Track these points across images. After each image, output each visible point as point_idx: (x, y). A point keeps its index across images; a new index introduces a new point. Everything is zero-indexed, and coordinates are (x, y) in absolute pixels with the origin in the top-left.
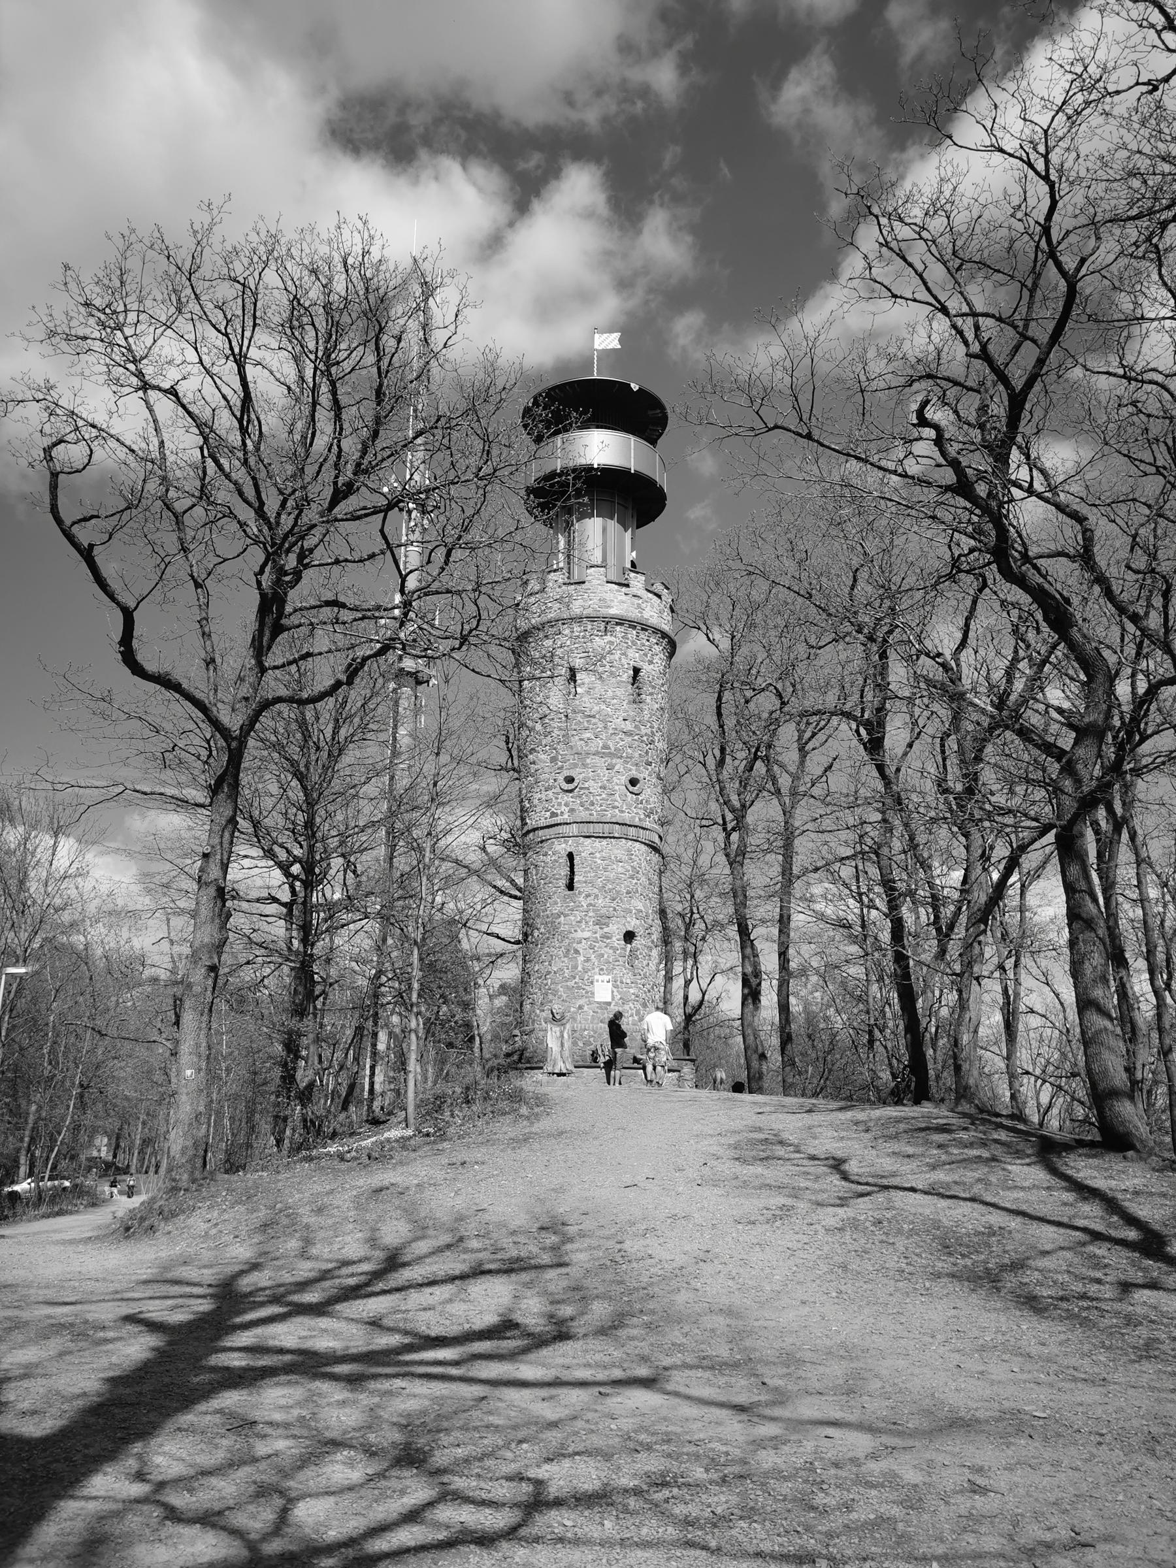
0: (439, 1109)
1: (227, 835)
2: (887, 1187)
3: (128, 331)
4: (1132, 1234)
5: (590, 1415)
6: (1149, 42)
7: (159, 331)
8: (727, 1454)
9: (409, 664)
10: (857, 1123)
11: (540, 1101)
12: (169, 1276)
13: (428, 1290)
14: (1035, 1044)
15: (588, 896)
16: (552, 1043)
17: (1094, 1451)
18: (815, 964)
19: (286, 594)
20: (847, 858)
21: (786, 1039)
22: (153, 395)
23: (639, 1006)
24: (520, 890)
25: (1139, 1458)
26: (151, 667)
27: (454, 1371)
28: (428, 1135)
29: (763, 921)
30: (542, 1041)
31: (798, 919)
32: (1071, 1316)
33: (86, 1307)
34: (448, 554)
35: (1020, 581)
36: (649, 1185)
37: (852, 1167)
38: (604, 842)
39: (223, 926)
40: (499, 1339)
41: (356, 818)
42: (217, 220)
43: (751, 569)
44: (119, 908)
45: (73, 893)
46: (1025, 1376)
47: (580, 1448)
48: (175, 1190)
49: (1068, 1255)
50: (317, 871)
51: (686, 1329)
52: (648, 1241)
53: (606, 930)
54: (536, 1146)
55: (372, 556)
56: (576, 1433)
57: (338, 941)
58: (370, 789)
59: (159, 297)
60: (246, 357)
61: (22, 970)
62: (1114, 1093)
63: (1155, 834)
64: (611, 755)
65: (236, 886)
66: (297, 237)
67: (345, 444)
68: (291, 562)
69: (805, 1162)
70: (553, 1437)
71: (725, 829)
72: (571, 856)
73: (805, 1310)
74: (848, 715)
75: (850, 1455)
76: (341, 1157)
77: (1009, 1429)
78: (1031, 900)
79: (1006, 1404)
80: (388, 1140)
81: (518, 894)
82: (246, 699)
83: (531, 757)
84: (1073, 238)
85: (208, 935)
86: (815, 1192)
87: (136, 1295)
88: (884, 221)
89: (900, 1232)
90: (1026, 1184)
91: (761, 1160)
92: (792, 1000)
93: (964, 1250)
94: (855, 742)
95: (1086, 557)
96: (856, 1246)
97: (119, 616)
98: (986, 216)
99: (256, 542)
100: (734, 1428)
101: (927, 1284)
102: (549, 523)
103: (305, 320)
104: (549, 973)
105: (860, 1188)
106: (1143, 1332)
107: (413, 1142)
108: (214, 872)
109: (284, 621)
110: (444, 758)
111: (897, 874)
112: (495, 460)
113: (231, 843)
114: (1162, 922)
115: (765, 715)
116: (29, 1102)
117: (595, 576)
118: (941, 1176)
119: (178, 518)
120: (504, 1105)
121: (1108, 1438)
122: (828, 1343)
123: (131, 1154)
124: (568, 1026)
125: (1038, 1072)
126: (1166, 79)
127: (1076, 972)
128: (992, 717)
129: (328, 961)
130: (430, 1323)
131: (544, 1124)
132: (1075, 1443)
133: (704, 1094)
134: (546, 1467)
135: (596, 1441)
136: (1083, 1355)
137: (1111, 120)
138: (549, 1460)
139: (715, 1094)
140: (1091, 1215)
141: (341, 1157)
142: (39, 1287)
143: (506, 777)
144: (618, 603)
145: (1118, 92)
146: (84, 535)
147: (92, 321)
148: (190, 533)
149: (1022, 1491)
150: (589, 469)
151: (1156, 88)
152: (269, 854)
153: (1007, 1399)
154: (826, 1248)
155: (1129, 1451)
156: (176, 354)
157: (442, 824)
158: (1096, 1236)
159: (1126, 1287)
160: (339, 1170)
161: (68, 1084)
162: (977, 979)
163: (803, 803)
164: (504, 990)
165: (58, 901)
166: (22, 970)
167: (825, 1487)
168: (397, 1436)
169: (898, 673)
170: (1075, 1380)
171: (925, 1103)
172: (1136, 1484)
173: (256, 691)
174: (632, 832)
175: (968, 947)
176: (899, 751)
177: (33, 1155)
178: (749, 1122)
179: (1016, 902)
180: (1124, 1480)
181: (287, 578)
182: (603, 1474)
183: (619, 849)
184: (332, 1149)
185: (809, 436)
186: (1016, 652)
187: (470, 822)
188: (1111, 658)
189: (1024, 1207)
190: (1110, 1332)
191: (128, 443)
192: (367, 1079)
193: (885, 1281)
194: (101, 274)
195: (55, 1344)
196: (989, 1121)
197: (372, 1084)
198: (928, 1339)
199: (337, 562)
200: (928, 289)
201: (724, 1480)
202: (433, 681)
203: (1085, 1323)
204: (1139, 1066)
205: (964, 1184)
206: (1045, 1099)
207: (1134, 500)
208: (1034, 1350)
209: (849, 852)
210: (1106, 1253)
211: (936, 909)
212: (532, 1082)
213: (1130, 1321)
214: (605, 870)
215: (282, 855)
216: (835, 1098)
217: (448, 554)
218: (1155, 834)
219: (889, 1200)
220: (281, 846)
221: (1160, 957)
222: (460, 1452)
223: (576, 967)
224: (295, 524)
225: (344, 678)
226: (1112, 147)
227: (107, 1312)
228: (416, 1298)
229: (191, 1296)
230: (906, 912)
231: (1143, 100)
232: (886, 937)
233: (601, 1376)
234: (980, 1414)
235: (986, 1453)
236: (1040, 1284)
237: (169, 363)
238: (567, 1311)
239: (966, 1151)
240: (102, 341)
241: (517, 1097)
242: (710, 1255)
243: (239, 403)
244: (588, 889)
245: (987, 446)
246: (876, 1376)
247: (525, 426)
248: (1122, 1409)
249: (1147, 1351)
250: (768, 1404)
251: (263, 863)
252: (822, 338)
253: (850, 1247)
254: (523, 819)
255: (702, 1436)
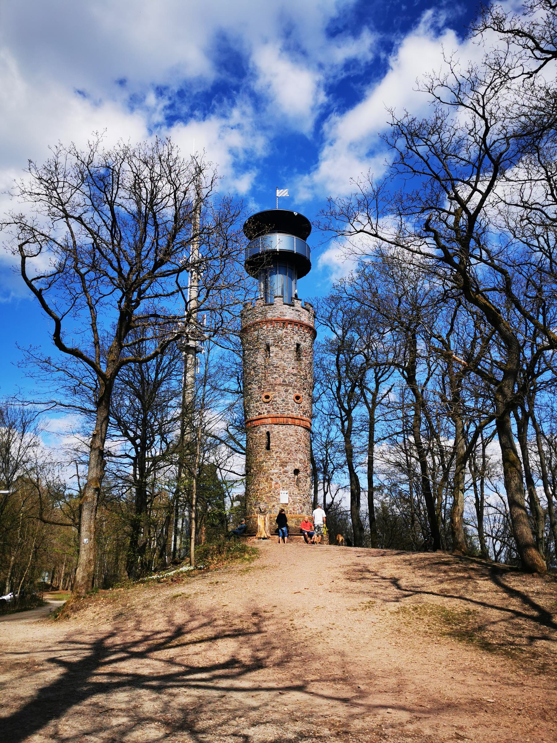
0: (206, 557)
1: (104, 426)
2: (420, 592)
3: (59, 191)
4: (535, 613)
5: (274, 704)
6: (528, 55)
7: (73, 191)
8: (340, 721)
9: (192, 343)
10: (405, 561)
11: (255, 551)
12: (70, 639)
13: (199, 645)
14: (492, 522)
15: (276, 452)
16: (260, 523)
17: (516, 718)
18: (386, 484)
19: (132, 312)
20: (399, 433)
21: (372, 520)
22: (71, 220)
23: (301, 505)
24: (244, 449)
25: (537, 721)
26: (68, 346)
27: (210, 684)
28: (200, 569)
29: (361, 464)
30: (256, 523)
31: (377, 463)
32: (507, 653)
33: (35, 654)
34: (208, 292)
35: (476, 302)
36: (306, 592)
37: (403, 583)
38: (284, 427)
39: (102, 470)
40: (232, 668)
41: (166, 416)
42: (100, 140)
43: (351, 297)
44: (53, 461)
45: (32, 454)
46: (485, 682)
47: (269, 720)
48: (78, 597)
49: (506, 624)
50: (148, 442)
51: (322, 662)
52: (305, 620)
53: (285, 469)
54: (252, 573)
55: (173, 293)
56: (268, 712)
57: (158, 475)
58: (172, 403)
59: (74, 175)
60: (114, 202)
61: (7, 492)
62: (528, 546)
63: (545, 420)
64: (287, 385)
65: (110, 450)
66: (137, 147)
67: (160, 242)
68: (135, 295)
69: (381, 580)
70: (254, 714)
71: (342, 420)
72: (268, 433)
73: (380, 652)
74: (398, 366)
75: (399, 721)
76: (158, 580)
77: (476, 708)
78: (488, 452)
79: (475, 696)
80: (182, 572)
81: (244, 452)
82: (114, 361)
83: (249, 386)
84: (497, 144)
85: (94, 473)
86: (384, 595)
87: (54, 649)
88: (409, 137)
89: (426, 613)
90: (486, 589)
91: (360, 579)
92: (375, 501)
93: (456, 621)
94: (402, 378)
95: (507, 290)
96: (405, 620)
97: (53, 323)
98: (457, 134)
99: (118, 288)
100: (342, 710)
101: (438, 638)
102: (256, 277)
103: (142, 185)
104: (258, 490)
105: (407, 593)
106: (541, 660)
107: (193, 573)
108: (98, 443)
109: (132, 324)
110: (208, 388)
111: (423, 440)
112: (229, 248)
113: (106, 429)
114: (550, 462)
115: (359, 366)
116: (11, 556)
117: (278, 301)
118: (445, 586)
119: (82, 276)
120: (237, 554)
121: (523, 711)
122: (390, 667)
123: (60, 581)
124: (268, 515)
125: (494, 535)
126: (536, 72)
127: (507, 486)
128: (464, 365)
129: (153, 485)
130: (198, 661)
131: (256, 563)
132: (507, 714)
133: (332, 547)
134: (252, 729)
135: (276, 716)
136: (512, 672)
137: (510, 91)
138: (254, 725)
139: (337, 547)
140: (515, 604)
141: (158, 580)
142: (12, 645)
143: (237, 396)
144: (289, 314)
145: (514, 78)
146: (36, 285)
147: (42, 186)
148: (88, 283)
149: (481, 738)
150: (274, 251)
151: (531, 76)
152: (126, 434)
153: (475, 693)
154: (390, 622)
155: (533, 718)
156: (81, 201)
157: (207, 419)
158: (518, 614)
159: (532, 639)
160: (157, 587)
161: (29, 547)
162: (462, 490)
163: (378, 407)
164: (238, 498)
165: (24, 458)
166: (7, 492)
167: (386, 737)
168: (179, 715)
169: (421, 346)
170: (508, 684)
171: (438, 551)
172: (536, 733)
173: (118, 357)
174: (297, 421)
175: (457, 475)
176: (423, 382)
177: (12, 581)
178: (354, 561)
179: (480, 453)
180: (530, 732)
181: (133, 304)
182: (279, 732)
183: (291, 430)
184: (155, 577)
185: (376, 235)
186: (475, 334)
187: (220, 418)
188: (520, 337)
189: (485, 601)
190: (524, 660)
191: (59, 242)
192: (173, 543)
193: (418, 637)
194: (46, 165)
195: (18, 672)
196: (469, 559)
197: (175, 545)
198: (438, 665)
199: (156, 296)
200: (430, 168)
201: (338, 734)
202: (203, 351)
203: (513, 657)
204: (540, 532)
205: (456, 589)
206: (497, 548)
207: (530, 263)
208: (489, 670)
209: (401, 430)
210: (524, 622)
211: (442, 457)
212: (251, 542)
213: (535, 655)
214: (285, 440)
215: (132, 434)
216: (397, 549)
217: (208, 292)
218: (545, 420)
219: (421, 598)
220: (131, 430)
221: (549, 478)
222: (211, 722)
223: (271, 487)
224: (137, 279)
225: (159, 350)
226: (512, 103)
227: (41, 657)
228: (192, 649)
229: (81, 649)
230: (429, 459)
231: (525, 82)
232: (419, 470)
233: (281, 685)
234: (462, 701)
235: (465, 720)
236: (492, 637)
237: (78, 205)
238: (261, 655)
239: (458, 574)
240: (47, 195)
241: (243, 550)
242: (334, 626)
243: (111, 224)
244: (276, 449)
245: (458, 240)
246: (413, 683)
247: (245, 232)
248: (530, 698)
249: (542, 669)
250: (356, 697)
251: (123, 439)
252: (381, 191)
253: (402, 621)
254: (245, 416)
255: (328, 713)
